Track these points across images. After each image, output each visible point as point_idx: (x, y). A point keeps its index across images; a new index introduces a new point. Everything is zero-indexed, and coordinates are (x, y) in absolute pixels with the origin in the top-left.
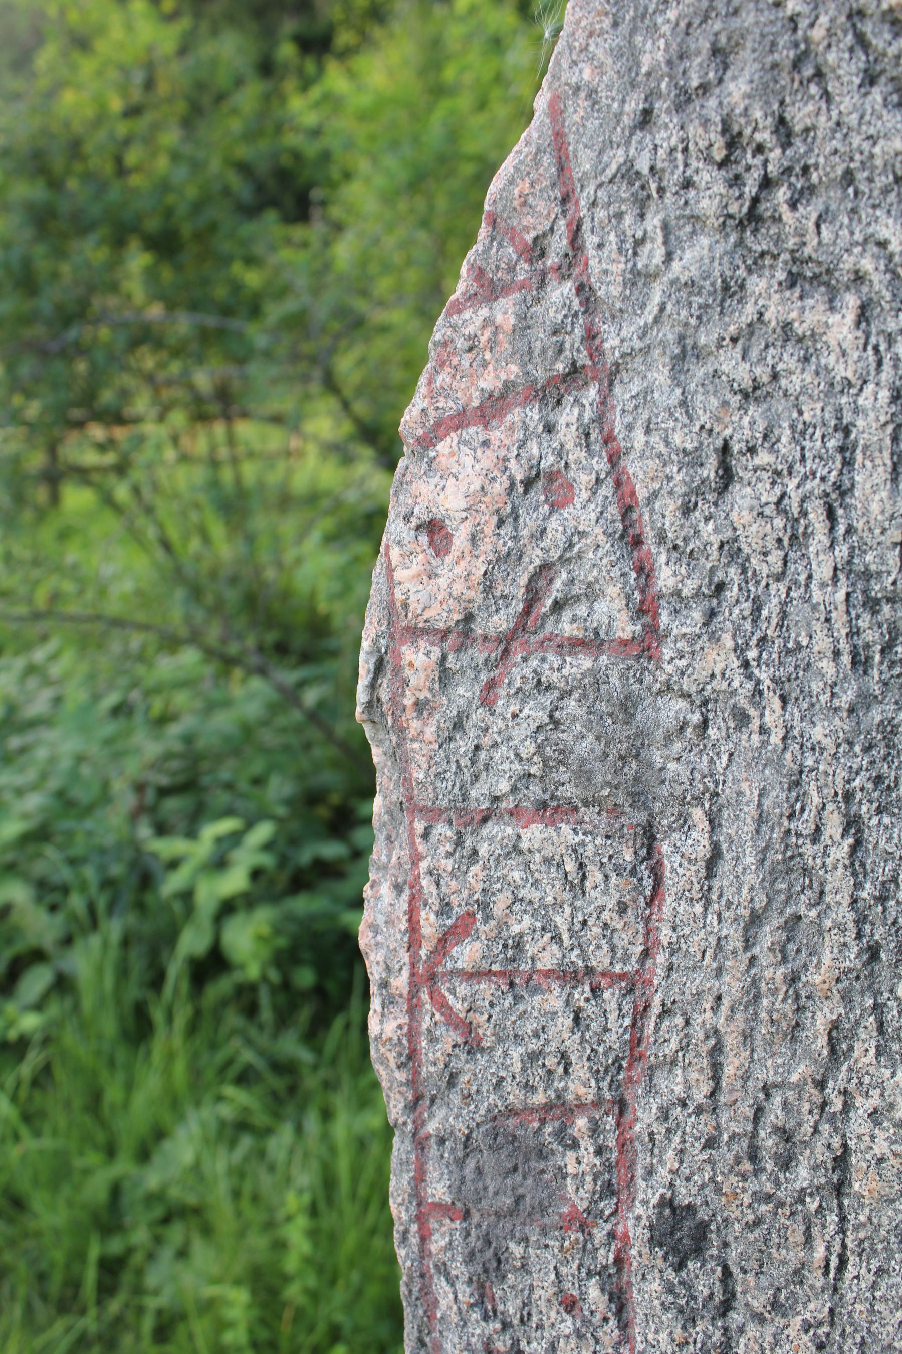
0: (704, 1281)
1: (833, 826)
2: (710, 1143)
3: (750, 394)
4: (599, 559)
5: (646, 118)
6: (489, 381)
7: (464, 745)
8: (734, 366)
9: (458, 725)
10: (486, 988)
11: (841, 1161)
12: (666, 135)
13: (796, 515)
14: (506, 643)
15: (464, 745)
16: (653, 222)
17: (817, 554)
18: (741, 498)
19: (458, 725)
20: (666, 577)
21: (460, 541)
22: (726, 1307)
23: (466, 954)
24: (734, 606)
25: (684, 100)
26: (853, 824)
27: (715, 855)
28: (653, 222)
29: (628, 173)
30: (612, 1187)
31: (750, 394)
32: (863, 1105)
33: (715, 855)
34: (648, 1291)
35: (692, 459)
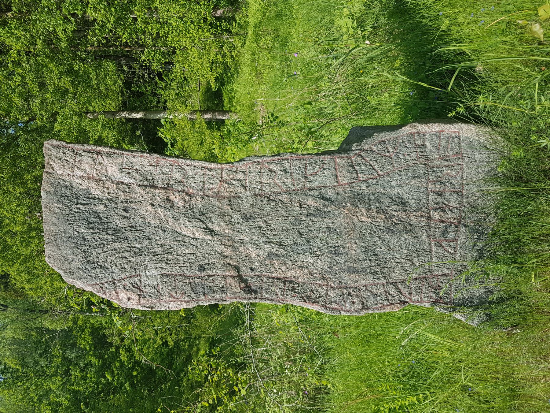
0: (207, 266)
1: (157, 257)
2: (191, 266)
3: (116, 266)
4: (131, 280)
5: (91, 276)
6: (114, 292)
7: (152, 295)
8: (114, 267)
9: (150, 296)
10: (178, 292)
11: (191, 254)
12: (92, 274)
13: (384, 217)
14: (140, 290)
15: (152, 295)
16: (100, 275)
17: (440, 194)
18: (126, 266)
19: (150, 296)
20: (134, 274)
21: (129, 296)
22: (209, 264)
23: (174, 294)
24: (136, 267)
25: (89, 272)
26: (157, 255)
27: (161, 268)
28: (100, 275)
29: (95, 278)
30: (199, 277)
31: (116, 266)
32: (184, 252)
33: (161, 268)
34: (210, 272)
35: (122, 271)
